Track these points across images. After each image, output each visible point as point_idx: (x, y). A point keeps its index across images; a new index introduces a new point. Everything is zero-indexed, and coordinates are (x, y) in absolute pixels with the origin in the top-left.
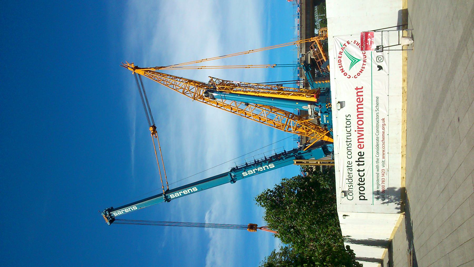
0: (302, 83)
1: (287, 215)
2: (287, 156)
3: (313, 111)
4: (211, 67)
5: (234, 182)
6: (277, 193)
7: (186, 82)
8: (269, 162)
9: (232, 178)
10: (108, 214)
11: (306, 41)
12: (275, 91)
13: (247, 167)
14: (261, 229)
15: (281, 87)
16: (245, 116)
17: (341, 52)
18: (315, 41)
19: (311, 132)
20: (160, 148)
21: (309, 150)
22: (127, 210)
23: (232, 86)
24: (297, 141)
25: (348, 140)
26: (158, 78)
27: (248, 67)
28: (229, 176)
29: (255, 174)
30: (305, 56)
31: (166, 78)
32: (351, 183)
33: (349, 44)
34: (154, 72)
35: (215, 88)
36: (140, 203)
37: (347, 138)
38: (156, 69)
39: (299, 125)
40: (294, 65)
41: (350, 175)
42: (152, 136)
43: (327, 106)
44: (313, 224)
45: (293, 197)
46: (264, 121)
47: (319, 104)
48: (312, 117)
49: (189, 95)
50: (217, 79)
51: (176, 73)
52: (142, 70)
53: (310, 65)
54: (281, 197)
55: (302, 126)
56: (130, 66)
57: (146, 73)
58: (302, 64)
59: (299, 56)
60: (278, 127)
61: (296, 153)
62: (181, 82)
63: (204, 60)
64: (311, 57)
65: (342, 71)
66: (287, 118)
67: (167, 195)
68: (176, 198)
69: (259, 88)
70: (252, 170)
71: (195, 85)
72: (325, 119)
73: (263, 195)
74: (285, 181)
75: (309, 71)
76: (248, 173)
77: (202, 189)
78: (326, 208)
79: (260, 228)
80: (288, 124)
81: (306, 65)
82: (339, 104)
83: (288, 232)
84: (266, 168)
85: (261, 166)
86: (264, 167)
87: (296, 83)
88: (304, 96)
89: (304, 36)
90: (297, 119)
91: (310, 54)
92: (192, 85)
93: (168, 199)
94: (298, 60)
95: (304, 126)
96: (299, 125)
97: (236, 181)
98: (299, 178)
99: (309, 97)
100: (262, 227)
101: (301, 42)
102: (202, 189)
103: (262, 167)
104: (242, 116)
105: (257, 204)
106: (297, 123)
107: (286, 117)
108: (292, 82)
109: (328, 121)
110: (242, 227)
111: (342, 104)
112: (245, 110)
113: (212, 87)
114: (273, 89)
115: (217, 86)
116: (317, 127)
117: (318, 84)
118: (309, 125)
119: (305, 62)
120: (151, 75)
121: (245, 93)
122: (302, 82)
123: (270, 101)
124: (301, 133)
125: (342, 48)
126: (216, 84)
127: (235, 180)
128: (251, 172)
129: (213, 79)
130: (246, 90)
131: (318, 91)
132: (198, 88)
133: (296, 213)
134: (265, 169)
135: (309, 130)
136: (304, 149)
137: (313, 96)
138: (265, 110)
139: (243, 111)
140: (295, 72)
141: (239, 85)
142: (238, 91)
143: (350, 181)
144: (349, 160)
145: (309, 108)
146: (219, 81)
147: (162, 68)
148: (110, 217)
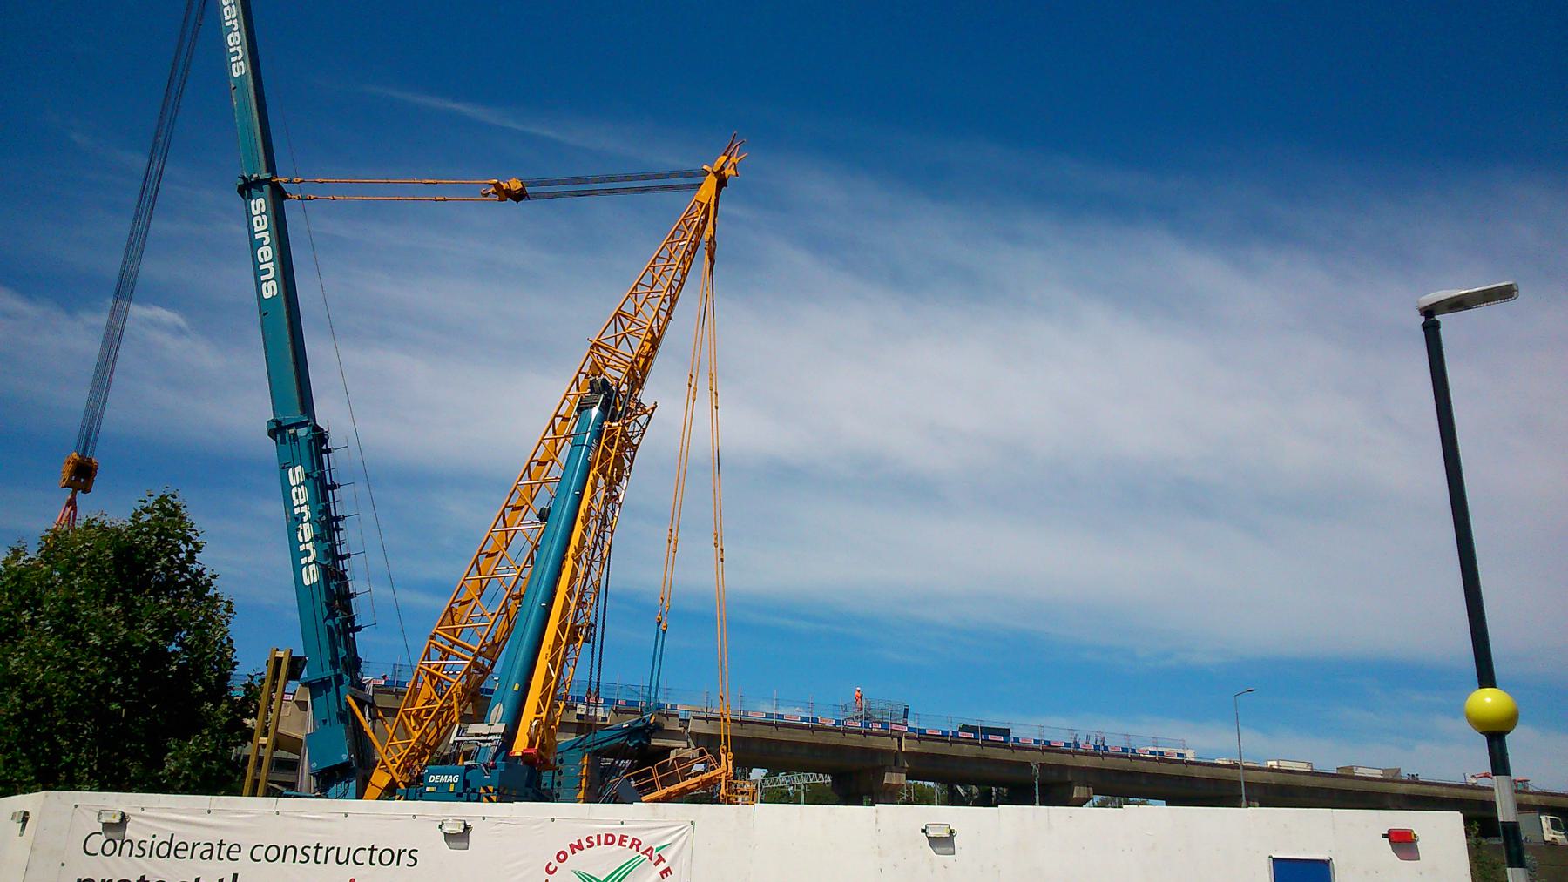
0: (594, 711)
1: (81, 604)
2: (339, 635)
3: (481, 741)
4: (689, 415)
5: (272, 433)
6: (181, 576)
7: (655, 330)
8: (326, 566)
9: (290, 427)
11: (726, 737)
12: (571, 615)
13: (322, 487)
14: (68, 505)
15: (581, 638)
16: (509, 505)
17: (637, 846)
18: (720, 765)
19: (414, 729)
20: (445, 200)
21: (346, 716)
22: (235, 41)
23: (612, 473)
24: (389, 678)
25: (322, 852)
26: (680, 241)
27: (671, 536)
28: (297, 416)
29: (288, 510)
30: (681, 729)
31: (675, 267)
32: (154, 850)
33: (662, 873)
34: (699, 232)
35: (616, 419)
36: (252, 91)
37: (333, 848)
38: (709, 242)
39: (445, 688)
40: (653, 690)
41: (187, 849)
42: (488, 182)
43: (488, 791)
44: (26, 697)
45: (150, 631)
46: (479, 569)
47: (498, 762)
48: (457, 736)
49: (610, 332)
50: (644, 430)
51: (689, 301)
52: (714, 198)
53: (644, 742)
54: (169, 585)
55: (441, 698)
56: (730, 163)
57: (701, 208)
58: (653, 718)
59: (684, 708)
60: (449, 614)
61: (346, 670)
62: (657, 312)
63: (716, 398)
64: (673, 748)
65: (576, 847)
66: (477, 649)
67: (266, 188)
68: (250, 216)
69: (593, 563)
70: (306, 503)
71: (641, 356)
72: (443, 779)
73: (180, 523)
74: (221, 610)
75: (625, 738)
76: (298, 486)
77: (265, 315)
78: (87, 752)
79: (72, 503)
80: (456, 650)
81: (646, 731)
82: (463, 826)
83: (23, 600)
84: (307, 553)
85: (315, 538)
86: (310, 547)
87: (589, 689)
88: (539, 711)
89: (744, 732)
90: (467, 683)
91: (686, 746)
92: (642, 346)
93: (249, 191)
94: (671, 705)
95: (438, 706)
96: (445, 688)
97: (276, 440)
98: (226, 665)
99: (533, 730)
100: (74, 509)
101: (725, 720)
102: (265, 315)
103: (311, 540)
104: (512, 494)
105: (147, 498)
106: (453, 682)
107: (481, 647)
108: (595, 679)
109: (433, 789)
110: (90, 432)
111: (458, 838)
112: (529, 507)
113: (620, 409)
114: (581, 610)
115: (619, 425)
116: (428, 751)
117: (579, 767)
118: (440, 725)
119: (658, 730)
120: (693, 222)
121: (581, 514)
122: (596, 713)
123: (539, 598)
124: (415, 693)
125: (651, 848)
126: (627, 421)
127: (279, 438)
128: (301, 496)
129: (647, 416)
130: (591, 518)
131: (546, 762)
132: (630, 365)
133: (83, 639)
134: (302, 548)
135: (420, 723)
136: (353, 698)
137: (531, 743)
138: (519, 577)
139: (529, 502)
140: (632, 693)
141: (612, 498)
142: (593, 491)
143: (164, 849)
144: (246, 851)
145: (495, 725)
146: (636, 433)
147: (708, 260)
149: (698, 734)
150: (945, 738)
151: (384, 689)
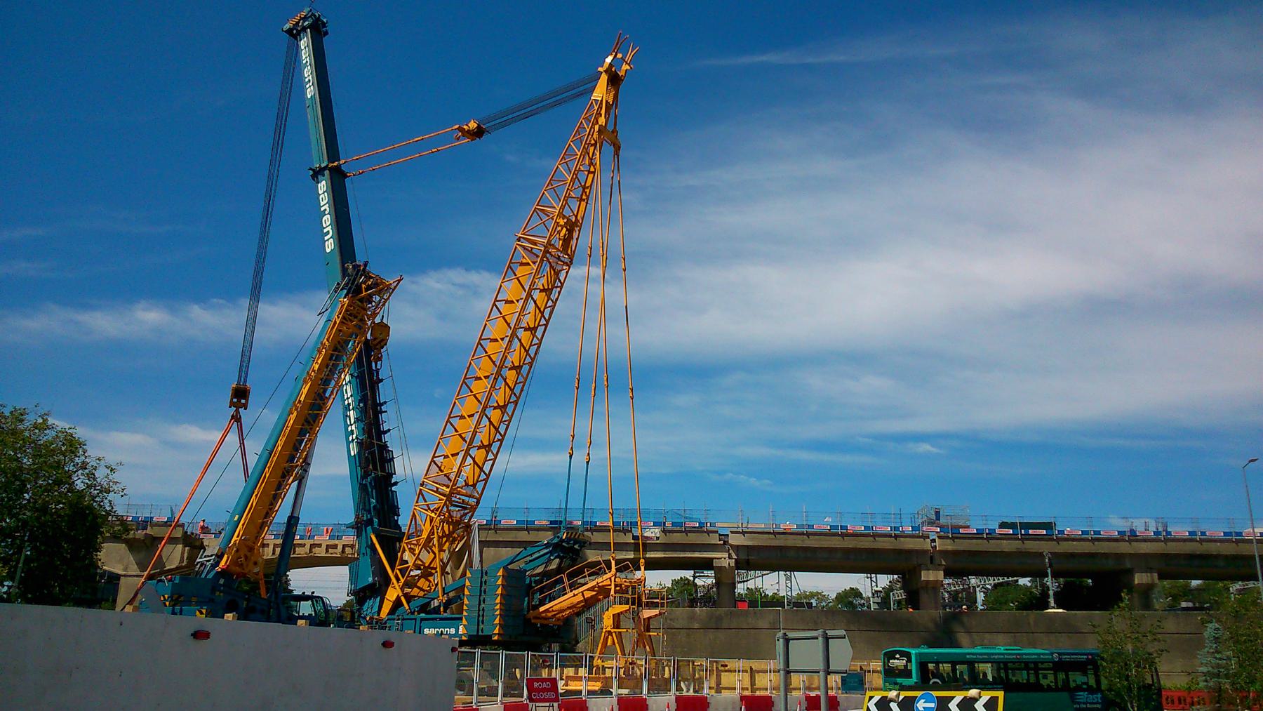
10: (305, 24)
67: (327, 172)
85: (357, 420)
93: (317, 178)
148: (299, 29)
149: (738, 546)
150: (980, 536)
151: (486, 527)
